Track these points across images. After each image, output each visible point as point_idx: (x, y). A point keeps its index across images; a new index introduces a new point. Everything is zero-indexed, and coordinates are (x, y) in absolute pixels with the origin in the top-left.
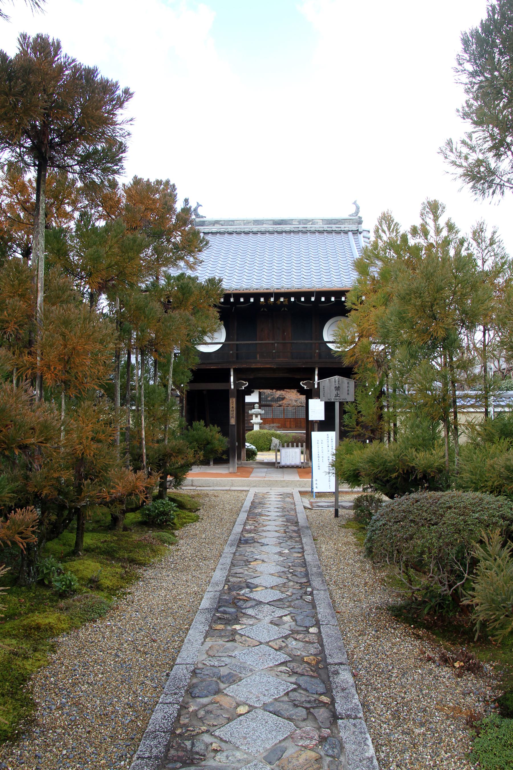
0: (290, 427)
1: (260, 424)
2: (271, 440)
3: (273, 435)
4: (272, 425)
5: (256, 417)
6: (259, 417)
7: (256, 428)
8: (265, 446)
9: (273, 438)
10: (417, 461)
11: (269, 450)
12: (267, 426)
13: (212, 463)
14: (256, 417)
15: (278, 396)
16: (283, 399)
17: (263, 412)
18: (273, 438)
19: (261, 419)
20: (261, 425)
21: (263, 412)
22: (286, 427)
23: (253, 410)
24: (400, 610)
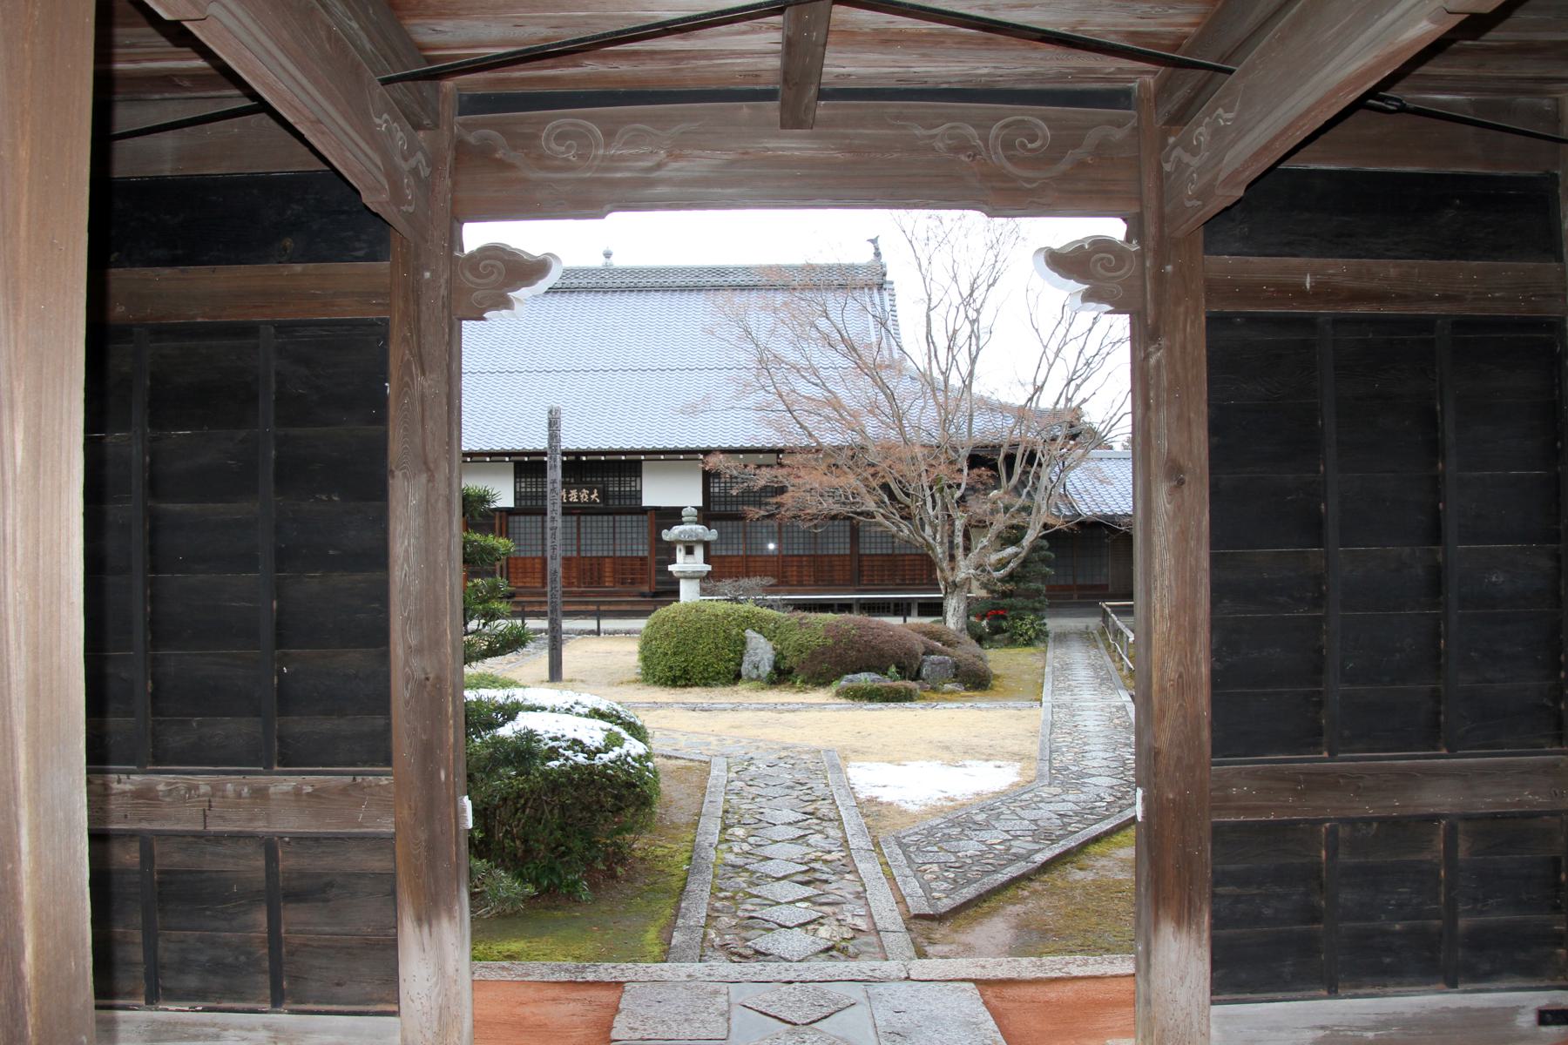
0: (800, 583)
1: (704, 578)
2: (744, 643)
3: (748, 621)
4: (745, 582)
5: (690, 551)
6: (699, 552)
7: (689, 593)
8: (721, 667)
9: (750, 633)
10: (542, 725)
11: (736, 677)
12: (727, 585)
13: (1248, 789)
14: (690, 551)
15: (762, 483)
16: (782, 490)
17: (712, 535)
18: (750, 633)
19: (706, 561)
20: (708, 582)
21: (712, 535)
22: (787, 583)
23: (677, 529)
24: (997, 630)
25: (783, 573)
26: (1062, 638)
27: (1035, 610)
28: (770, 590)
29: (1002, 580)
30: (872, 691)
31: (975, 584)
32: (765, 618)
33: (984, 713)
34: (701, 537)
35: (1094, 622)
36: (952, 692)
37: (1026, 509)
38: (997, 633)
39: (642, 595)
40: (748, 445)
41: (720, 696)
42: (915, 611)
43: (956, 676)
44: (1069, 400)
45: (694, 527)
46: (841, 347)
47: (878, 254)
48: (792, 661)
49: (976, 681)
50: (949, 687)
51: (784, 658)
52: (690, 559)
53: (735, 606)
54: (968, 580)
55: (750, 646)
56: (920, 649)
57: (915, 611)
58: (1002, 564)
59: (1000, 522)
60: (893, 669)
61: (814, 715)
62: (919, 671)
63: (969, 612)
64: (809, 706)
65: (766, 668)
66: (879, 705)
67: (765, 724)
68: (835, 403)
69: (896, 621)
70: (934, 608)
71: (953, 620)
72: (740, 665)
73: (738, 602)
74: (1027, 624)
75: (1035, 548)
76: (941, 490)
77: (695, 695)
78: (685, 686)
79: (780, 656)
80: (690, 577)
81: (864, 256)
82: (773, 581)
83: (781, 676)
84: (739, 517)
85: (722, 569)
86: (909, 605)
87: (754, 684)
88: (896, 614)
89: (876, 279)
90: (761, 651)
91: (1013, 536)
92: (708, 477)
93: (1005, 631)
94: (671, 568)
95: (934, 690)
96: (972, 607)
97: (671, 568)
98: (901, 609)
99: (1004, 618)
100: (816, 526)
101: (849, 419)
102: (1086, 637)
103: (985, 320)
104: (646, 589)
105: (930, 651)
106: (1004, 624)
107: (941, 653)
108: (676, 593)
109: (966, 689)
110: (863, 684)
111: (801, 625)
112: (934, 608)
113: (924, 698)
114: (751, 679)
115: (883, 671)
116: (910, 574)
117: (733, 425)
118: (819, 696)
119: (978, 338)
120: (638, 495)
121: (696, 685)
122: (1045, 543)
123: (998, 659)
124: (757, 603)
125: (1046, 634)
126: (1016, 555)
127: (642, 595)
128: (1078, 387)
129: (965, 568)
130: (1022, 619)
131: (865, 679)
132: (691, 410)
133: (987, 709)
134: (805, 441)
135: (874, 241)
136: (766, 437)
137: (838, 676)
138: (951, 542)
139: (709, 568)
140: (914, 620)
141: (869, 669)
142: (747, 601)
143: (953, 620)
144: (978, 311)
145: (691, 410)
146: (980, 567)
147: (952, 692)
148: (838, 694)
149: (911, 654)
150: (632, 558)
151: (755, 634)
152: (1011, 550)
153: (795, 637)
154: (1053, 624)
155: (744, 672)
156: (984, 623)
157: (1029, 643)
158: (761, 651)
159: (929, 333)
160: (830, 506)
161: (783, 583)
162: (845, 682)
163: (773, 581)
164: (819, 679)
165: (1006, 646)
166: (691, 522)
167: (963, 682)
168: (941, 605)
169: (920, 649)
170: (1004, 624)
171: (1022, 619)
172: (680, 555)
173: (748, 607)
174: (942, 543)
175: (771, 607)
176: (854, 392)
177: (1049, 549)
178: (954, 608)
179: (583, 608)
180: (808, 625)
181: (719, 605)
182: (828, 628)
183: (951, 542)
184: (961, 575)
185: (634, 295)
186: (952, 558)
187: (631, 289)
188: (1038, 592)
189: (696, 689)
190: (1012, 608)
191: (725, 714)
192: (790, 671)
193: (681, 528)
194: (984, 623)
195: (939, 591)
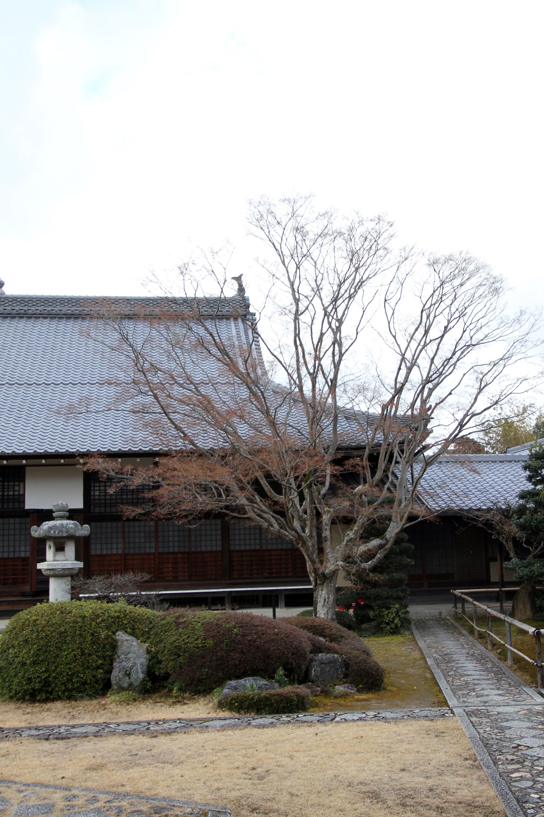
0: (175, 579)
2: (114, 646)
3: (119, 622)
4: (118, 579)
5: (60, 548)
6: (70, 549)
7: (58, 592)
8: (88, 676)
9: (121, 636)
12: (98, 584)
14: (60, 548)
16: (157, 487)
17: (85, 530)
18: (121, 636)
19: (77, 559)
20: (78, 580)
25: (159, 569)
26: (423, 625)
27: (398, 599)
28: (142, 586)
29: (374, 569)
30: (260, 700)
31: (341, 574)
32: (138, 620)
33: (392, 727)
34: (72, 532)
35: (445, 609)
36: (344, 696)
37: (390, 502)
38: (362, 622)
39: (24, 594)
40: (126, 448)
41: (85, 714)
42: (282, 602)
43: (346, 676)
44: (424, 402)
45: (65, 522)
46: (214, 350)
47: (241, 290)
48: (168, 665)
49: (368, 680)
50: (340, 689)
51: (159, 662)
52: (60, 556)
53: (105, 605)
54: (335, 573)
55: (122, 649)
56: (307, 647)
57: (282, 602)
58: (368, 556)
59: (363, 516)
60: (281, 672)
61: (194, 738)
62: (307, 672)
63: (338, 602)
64: (188, 725)
65: (139, 675)
66: (268, 719)
67: (133, 760)
68: (207, 405)
69: (267, 612)
70: (305, 599)
71: (323, 610)
72: (110, 672)
73: (110, 601)
74: (389, 615)
75: (398, 541)
76: (309, 486)
77: (53, 715)
78: (46, 701)
79: (154, 660)
80: (60, 574)
81: (231, 292)
82: (147, 577)
83: (155, 684)
84: (117, 518)
85: (93, 564)
86: (277, 596)
87: (124, 695)
88: (265, 605)
89: (241, 311)
90: (133, 654)
91: (374, 529)
92: (90, 479)
93: (372, 620)
94: (40, 566)
95: (326, 693)
96: (342, 599)
97: (40, 566)
98: (269, 600)
99: (370, 607)
100: (189, 523)
101: (220, 421)
102: (441, 621)
103: (347, 330)
104: (27, 588)
105: (317, 649)
106: (371, 614)
107: (329, 650)
108: (46, 592)
109: (359, 691)
110: (249, 693)
111: (178, 624)
112: (305, 599)
113: (317, 705)
114: (121, 689)
115: (268, 674)
116: (281, 568)
117: (109, 430)
118: (198, 709)
119: (340, 345)
120: (21, 499)
121: (59, 698)
122: (405, 536)
123: (383, 650)
124: (130, 601)
125: (409, 621)
126: (381, 547)
127: (24, 594)
128: (431, 391)
129: (333, 561)
130: (388, 608)
131: (250, 685)
132: (71, 412)
133: (395, 720)
134: (180, 444)
135: (238, 279)
136: (143, 440)
137: (220, 683)
138: (319, 535)
139: (80, 565)
140: (283, 612)
141: (254, 673)
142: (119, 598)
143: (323, 610)
144: (340, 321)
145: (71, 412)
146: (348, 559)
147: (344, 696)
148: (221, 705)
149: (298, 653)
150: (15, 559)
151: (126, 637)
152: (375, 542)
153: (171, 638)
154: (417, 611)
155: (113, 682)
156: (351, 611)
157: (395, 631)
158: (133, 654)
159: (297, 335)
160: (205, 503)
161: (158, 579)
162: (227, 690)
163: (147, 577)
164: (198, 686)
165: (374, 634)
166: (61, 518)
167: (355, 683)
168: (312, 595)
169: (307, 647)
170: (371, 614)
171: (388, 608)
172: (50, 553)
173: (121, 605)
174: (311, 536)
175: (145, 604)
176: (228, 394)
177: (409, 541)
178: (323, 597)
179: (279, 580)
180: (186, 625)
181: (89, 606)
182: (208, 627)
183: (319, 535)
184: (329, 567)
185: (24, 320)
186: (321, 551)
187: (21, 316)
188: (401, 581)
189: (58, 705)
190: (377, 597)
191: (351, 308)
192: (166, 677)
193: (51, 523)
194: (351, 611)
195: (309, 583)
